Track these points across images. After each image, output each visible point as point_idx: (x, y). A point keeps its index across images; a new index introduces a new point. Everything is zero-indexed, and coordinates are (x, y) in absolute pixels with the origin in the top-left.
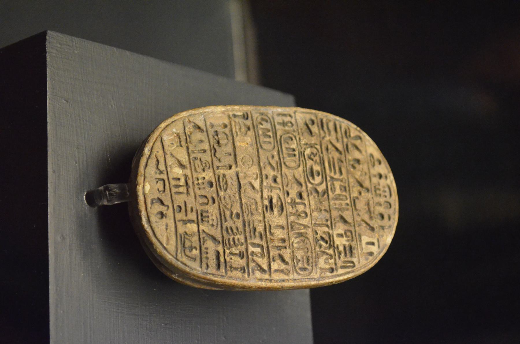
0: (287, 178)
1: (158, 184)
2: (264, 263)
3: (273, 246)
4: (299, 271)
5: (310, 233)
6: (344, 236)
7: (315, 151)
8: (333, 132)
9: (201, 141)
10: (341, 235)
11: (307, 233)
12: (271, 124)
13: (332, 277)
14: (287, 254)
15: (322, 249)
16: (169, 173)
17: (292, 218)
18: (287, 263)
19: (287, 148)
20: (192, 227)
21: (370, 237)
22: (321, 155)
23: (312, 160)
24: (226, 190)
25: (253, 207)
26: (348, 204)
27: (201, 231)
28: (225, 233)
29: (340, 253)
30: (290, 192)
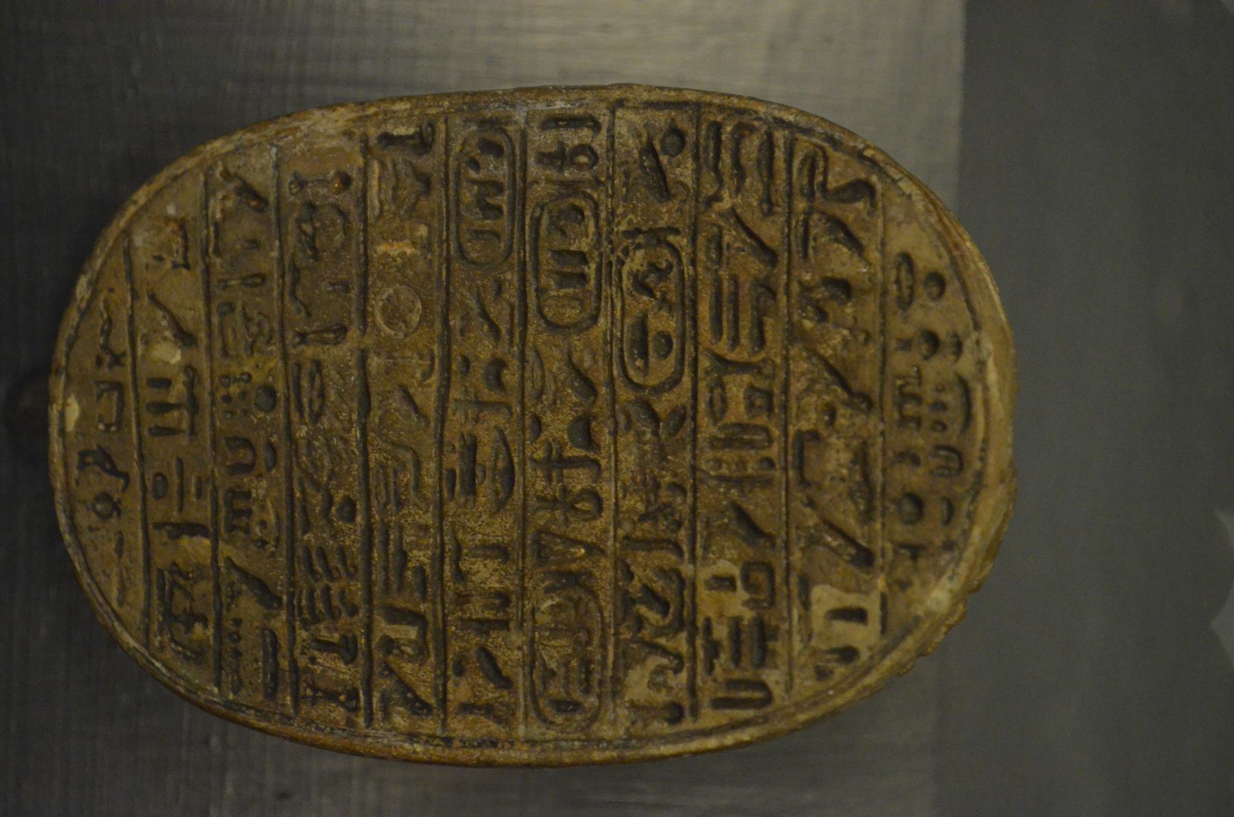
0: (542, 366)
1: (104, 400)
2: (422, 678)
3: (461, 619)
4: (549, 711)
5: (605, 574)
6: (739, 583)
7: (665, 257)
8: (753, 181)
9: (254, 244)
10: (725, 583)
11: (590, 575)
12: (512, 164)
13: (678, 738)
14: (510, 649)
15: (646, 633)
16: (139, 361)
17: (542, 518)
18: (506, 683)
19: (559, 254)
20: (197, 548)
21: (848, 590)
22: (689, 271)
23: (650, 293)
24: (316, 417)
25: (408, 477)
26: (770, 463)
27: (222, 564)
28: (300, 568)
29: (713, 649)
30: (547, 418)
